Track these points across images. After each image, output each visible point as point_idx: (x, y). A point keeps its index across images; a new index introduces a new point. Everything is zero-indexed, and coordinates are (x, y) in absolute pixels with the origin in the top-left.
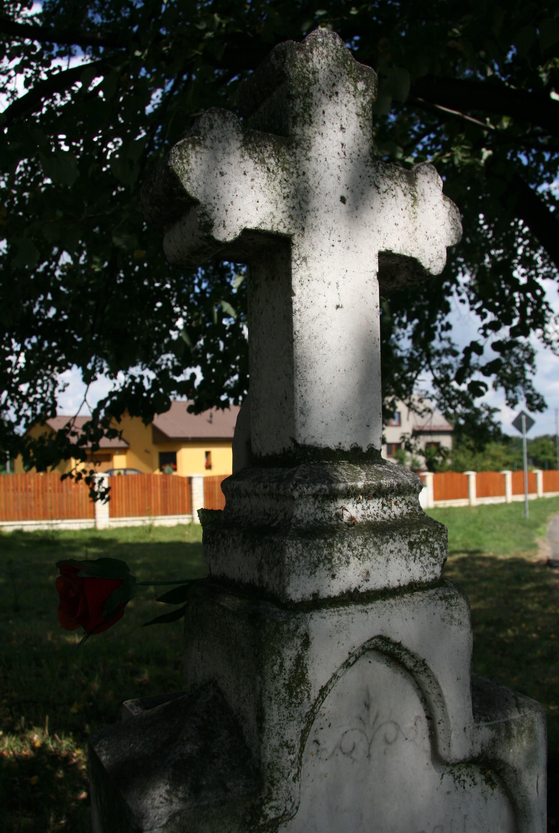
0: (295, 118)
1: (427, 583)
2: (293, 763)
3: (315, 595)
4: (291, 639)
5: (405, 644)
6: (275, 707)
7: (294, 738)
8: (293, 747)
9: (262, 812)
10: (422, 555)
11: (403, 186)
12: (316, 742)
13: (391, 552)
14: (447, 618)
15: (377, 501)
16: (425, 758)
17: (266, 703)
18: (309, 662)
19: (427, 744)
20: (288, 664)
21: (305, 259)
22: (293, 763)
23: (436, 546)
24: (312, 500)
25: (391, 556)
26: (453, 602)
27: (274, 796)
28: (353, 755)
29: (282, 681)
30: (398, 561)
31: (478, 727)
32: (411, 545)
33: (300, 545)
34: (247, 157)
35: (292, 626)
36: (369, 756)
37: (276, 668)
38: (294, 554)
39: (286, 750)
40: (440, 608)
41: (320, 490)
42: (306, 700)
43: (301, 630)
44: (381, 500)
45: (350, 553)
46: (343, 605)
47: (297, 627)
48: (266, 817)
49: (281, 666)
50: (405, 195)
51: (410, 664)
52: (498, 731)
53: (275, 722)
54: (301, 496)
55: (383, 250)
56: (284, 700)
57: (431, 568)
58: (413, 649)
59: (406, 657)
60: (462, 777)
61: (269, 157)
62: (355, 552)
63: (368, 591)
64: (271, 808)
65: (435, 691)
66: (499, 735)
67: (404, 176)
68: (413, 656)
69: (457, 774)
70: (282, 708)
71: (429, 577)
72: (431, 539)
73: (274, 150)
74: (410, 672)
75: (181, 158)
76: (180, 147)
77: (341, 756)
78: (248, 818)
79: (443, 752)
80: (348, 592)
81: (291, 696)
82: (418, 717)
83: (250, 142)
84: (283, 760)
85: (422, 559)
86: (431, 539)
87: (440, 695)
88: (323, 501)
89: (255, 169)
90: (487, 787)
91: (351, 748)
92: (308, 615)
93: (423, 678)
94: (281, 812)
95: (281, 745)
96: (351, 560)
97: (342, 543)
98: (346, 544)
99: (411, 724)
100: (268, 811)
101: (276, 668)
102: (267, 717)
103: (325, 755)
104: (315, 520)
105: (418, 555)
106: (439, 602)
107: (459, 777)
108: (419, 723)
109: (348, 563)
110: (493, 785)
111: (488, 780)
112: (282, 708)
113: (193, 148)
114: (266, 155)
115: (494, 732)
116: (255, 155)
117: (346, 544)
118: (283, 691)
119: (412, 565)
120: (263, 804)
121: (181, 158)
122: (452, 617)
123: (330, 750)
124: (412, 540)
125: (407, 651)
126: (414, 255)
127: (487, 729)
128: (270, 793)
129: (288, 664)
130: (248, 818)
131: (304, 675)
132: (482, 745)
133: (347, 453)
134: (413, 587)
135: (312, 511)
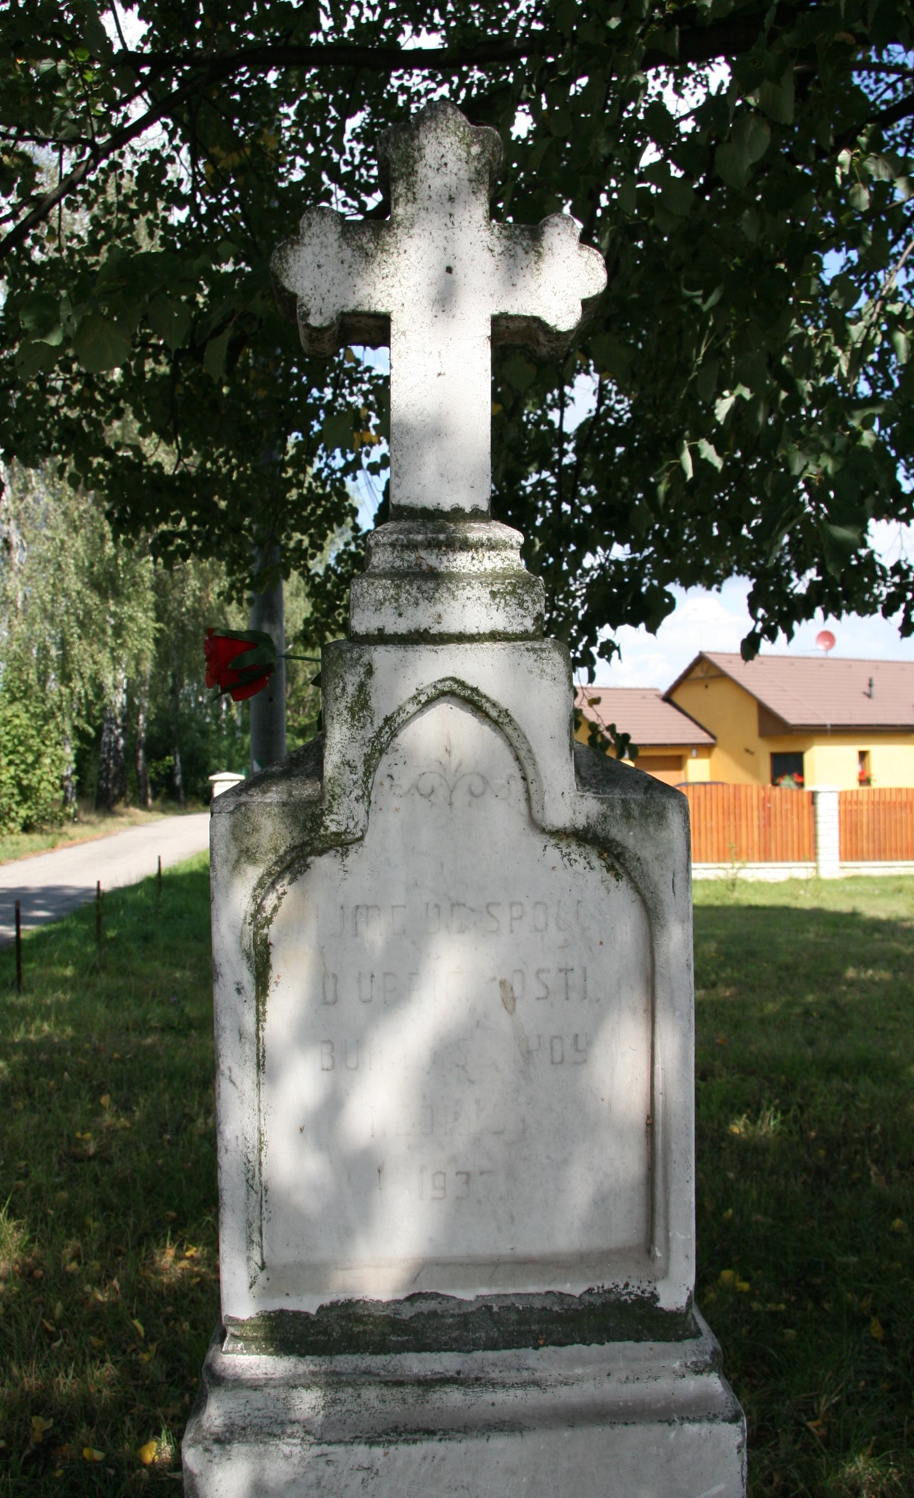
0: (397, 200)
1: (514, 634)
2: (355, 783)
3: (381, 630)
4: (354, 666)
5: (483, 690)
6: (337, 726)
7: (356, 759)
8: (356, 767)
9: (322, 823)
10: (506, 605)
11: (525, 244)
12: (391, 777)
13: (468, 598)
14: (537, 671)
15: (466, 554)
16: (520, 823)
17: (328, 721)
18: (373, 690)
19: (523, 806)
20: (351, 689)
21: (404, 333)
22: (355, 783)
23: (526, 598)
24: (390, 549)
25: (468, 602)
26: (544, 655)
27: (335, 810)
28: (432, 798)
29: (344, 704)
30: (476, 608)
31: (582, 796)
32: (493, 594)
33: (365, 584)
34: (345, 247)
35: (355, 655)
36: (451, 804)
37: (338, 691)
38: (359, 591)
39: (347, 768)
40: (529, 659)
41: (397, 540)
42: (369, 725)
43: (365, 659)
44: (470, 554)
45: (419, 595)
46: (412, 644)
47: (361, 657)
48: (326, 828)
49: (344, 689)
50: (527, 253)
51: (494, 713)
52: (612, 806)
53: (337, 740)
54: (377, 544)
55: (496, 313)
56: (346, 721)
57: (519, 620)
58: (493, 696)
59: (487, 706)
60: (573, 856)
61: (368, 242)
62: (426, 595)
63: (440, 634)
64: (332, 820)
65: (524, 746)
66: (612, 811)
67: (527, 233)
68: (494, 705)
69: (565, 850)
70: (344, 728)
71: (519, 629)
72: (519, 591)
73: (374, 234)
74: (496, 724)
75: (280, 259)
76: (279, 249)
77: (417, 796)
78: (309, 825)
79: (538, 816)
80: (417, 631)
81: (353, 718)
82: (511, 776)
83: (349, 231)
84: (345, 777)
85: (507, 609)
86: (519, 591)
87: (530, 751)
88: (402, 551)
89: (353, 256)
90: (609, 876)
91: (429, 791)
92: (372, 648)
93: (509, 730)
94: (343, 828)
95: (342, 763)
96: (421, 601)
97: (411, 586)
98: (415, 587)
99: (504, 782)
100: (328, 823)
101: (338, 691)
102: (328, 734)
103: (398, 791)
104: (393, 567)
105: (502, 605)
106: (526, 653)
107: (569, 854)
108: (512, 782)
109: (417, 604)
110: (618, 877)
111: (610, 868)
112: (344, 728)
113: (292, 247)
114: (365, 241)
115: (605, 806)
116: (354, 243)
117: (415, 587)
118: (345, 712)
119: (494, 613)
120: (323, 814)
121: (280, 259)
122: (543, 671)
123: (406, 787)
124: (495, 589)
125: (488, 700)
126: (536, 314)
127: (595, 801)
128: (331, 806)
129: (351, 689)
130: (309, 825)
131: (366, 702)
132: (588, 817)
133: (447, 513)
134: (494, 636)
135: (391, 559)
